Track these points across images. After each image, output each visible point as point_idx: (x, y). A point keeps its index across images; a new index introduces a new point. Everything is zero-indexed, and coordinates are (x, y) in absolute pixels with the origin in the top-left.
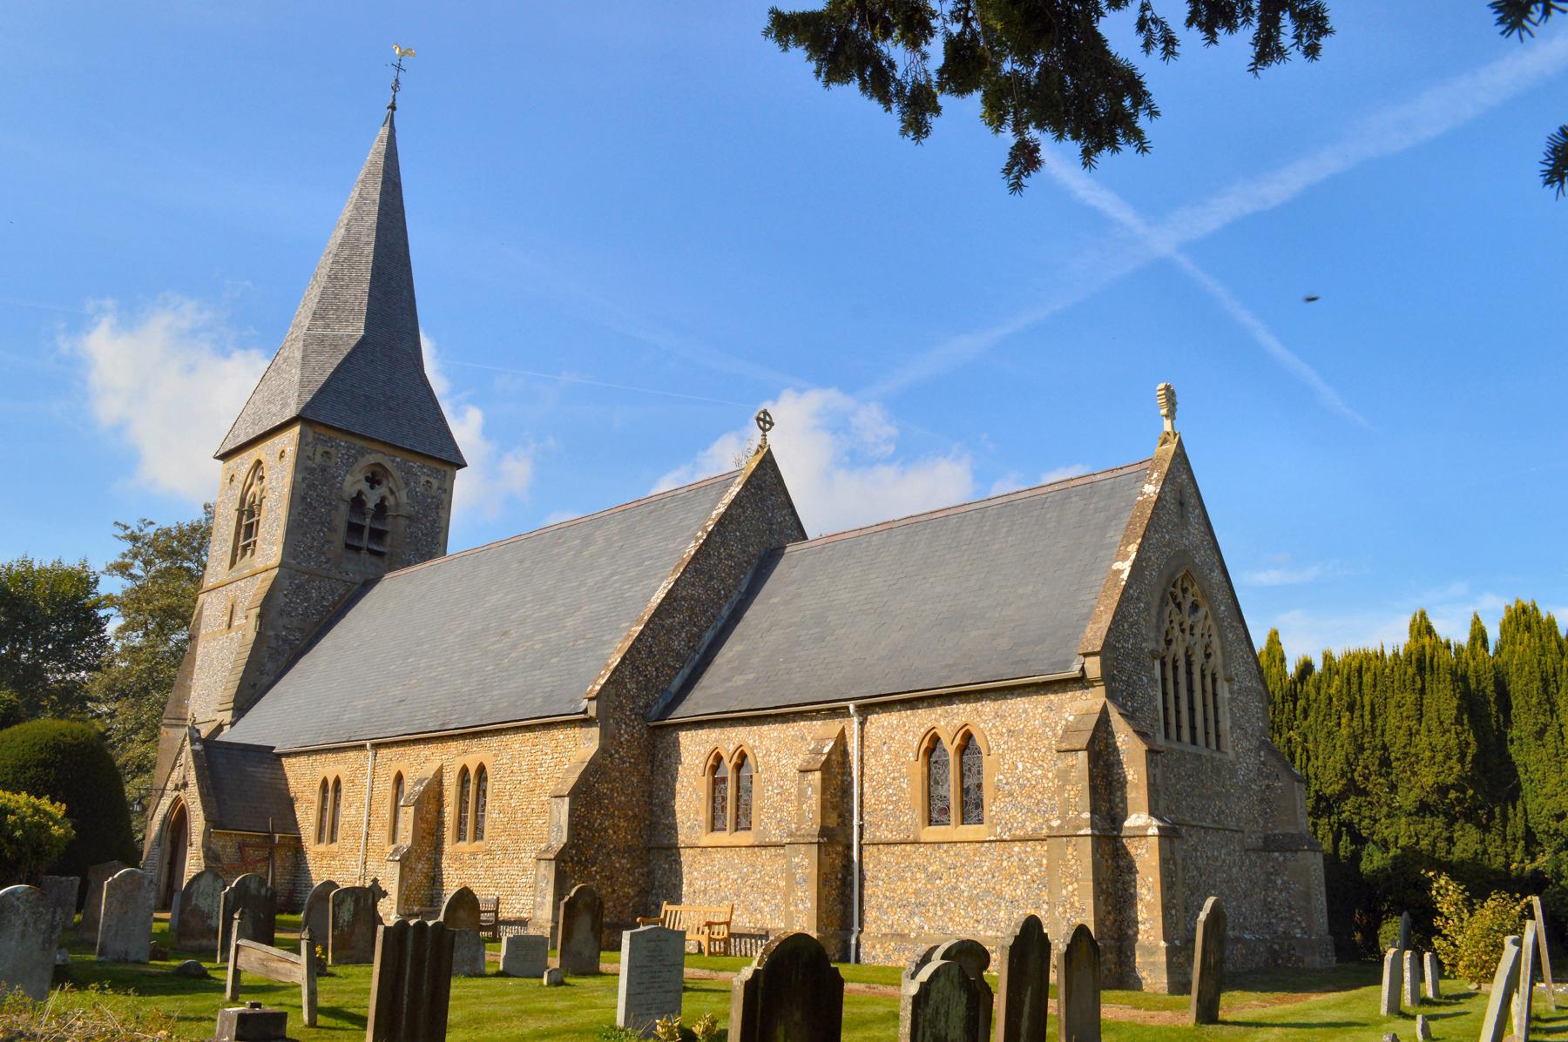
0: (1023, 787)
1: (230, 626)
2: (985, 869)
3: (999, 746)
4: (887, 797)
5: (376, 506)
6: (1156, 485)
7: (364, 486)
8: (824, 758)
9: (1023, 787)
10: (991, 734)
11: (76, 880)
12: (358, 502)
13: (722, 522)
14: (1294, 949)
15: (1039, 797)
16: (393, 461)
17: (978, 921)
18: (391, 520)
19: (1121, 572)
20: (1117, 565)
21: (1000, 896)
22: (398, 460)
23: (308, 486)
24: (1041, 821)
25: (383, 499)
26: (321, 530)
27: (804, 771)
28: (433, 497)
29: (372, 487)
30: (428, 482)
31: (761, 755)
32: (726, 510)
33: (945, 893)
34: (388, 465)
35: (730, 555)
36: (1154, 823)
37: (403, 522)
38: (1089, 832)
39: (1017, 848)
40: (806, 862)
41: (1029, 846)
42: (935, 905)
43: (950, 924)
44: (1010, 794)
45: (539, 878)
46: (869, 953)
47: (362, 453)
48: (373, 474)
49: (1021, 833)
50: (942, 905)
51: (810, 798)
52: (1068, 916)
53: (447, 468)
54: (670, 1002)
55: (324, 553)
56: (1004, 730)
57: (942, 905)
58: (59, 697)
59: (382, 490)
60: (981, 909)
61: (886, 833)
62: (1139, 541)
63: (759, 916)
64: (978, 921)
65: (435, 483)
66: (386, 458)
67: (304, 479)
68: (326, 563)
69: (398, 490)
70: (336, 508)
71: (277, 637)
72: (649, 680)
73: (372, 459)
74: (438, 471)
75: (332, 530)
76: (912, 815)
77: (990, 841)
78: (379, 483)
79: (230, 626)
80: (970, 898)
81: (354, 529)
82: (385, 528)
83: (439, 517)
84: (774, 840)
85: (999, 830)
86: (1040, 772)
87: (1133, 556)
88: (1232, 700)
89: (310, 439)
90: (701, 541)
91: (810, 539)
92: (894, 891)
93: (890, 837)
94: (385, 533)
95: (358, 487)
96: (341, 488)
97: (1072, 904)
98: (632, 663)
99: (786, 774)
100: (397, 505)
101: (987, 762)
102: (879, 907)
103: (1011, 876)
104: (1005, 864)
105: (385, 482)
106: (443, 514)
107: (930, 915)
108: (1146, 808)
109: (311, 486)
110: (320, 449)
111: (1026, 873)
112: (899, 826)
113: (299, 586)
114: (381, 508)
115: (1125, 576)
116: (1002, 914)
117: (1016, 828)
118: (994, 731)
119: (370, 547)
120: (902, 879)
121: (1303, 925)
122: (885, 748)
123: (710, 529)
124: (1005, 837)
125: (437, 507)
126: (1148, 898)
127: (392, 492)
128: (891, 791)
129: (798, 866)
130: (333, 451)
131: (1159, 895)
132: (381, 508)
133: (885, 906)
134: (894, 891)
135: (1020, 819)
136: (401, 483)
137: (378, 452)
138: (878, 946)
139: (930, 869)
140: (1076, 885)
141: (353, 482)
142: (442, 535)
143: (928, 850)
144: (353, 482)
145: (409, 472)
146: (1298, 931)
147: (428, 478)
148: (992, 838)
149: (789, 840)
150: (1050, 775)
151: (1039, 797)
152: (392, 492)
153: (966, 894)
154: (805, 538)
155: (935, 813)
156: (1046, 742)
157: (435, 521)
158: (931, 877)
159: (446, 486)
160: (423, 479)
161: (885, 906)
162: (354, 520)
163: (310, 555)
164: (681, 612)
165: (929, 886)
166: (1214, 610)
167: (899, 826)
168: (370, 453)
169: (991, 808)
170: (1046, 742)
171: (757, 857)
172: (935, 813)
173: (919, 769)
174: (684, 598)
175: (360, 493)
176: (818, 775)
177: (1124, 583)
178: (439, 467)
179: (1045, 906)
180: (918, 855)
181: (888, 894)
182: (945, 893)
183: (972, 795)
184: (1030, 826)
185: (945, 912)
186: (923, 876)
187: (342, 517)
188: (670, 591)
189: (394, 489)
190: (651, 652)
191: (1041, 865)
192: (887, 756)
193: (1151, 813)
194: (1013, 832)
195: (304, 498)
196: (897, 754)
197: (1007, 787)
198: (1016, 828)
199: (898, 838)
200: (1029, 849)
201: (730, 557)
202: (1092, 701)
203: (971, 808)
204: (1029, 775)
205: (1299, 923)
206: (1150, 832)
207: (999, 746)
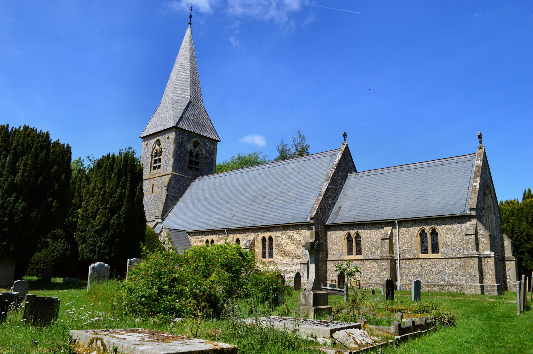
0: (451, 244)
1: (152, 192)
2: (440, 265)
3: (444, 233)
4: (408, 246)
5: (196, 154)
6: (481, 161)
7: (193, 148)
8: (389, 235)
9: (451, 244)
10: (441, 230)
11: (482, 259)
12: (191, 153)
13: (339, 165)
14: (511, 287)
15: (457, 246)
16: (201, 140)
17: (438, 279)
18: (200, 158)
19: (476, 186)
20: (474, 184)
21: (445, 273)
22: (202, 139)
23: (178, 148)
24: (457, 253)
25: (198, 152)
26: (182, 162)
27: (383, 239)
28: (212, 151)
29: (195, 148)
30: (210, 146)
31: (364, 234)
32: (339, 162)
33: (427, 272)
34: (199, 141)
35: (340, 175)
36: (493, 253)
37: (204, 159)
38: (493, 256)
39: (450, 260)
40: (386, 264)
41: (454, 260)
42: (425, 275)
43: (429, 280)
44: (448, 245)
45: (301, 269)
46: (403, 289)
47: (192, 138)
48: (195, 144)
49: (451, 256)
50: (427, 275)
51: (385, 246)
52: (471, 277)
53: (215, 142)
54: (58, 336)
55: (183, 169)
56: (445, 228)
57: (427, 275)
58: (526, 237)
59: (198, 149)
60: (439, 276)
61: (408, 256)
62: (480, 177)
63: (366, 279)
64: (438, 279)
65: (212, 146)
66: (199, 139)
67: (177, 146)
68: (184, 172)
69: (202, 149)
70: (186, 155)
71: (172, 196)
72: (324, 212)
73: (195, 139)
74: (213, 143)
75: (185, 162)
76: (416, 250)
77: (442, 258)
78: (196, 147)
79: (152, 192)
80: (436, 273)
81: (191, 162)
82: (199, 161)
83: (213, 157)
84: (370, 258)
85: (444, 255)
86: (457, 240)
87: (479, 182)
88: (495, 220)
89: (178, 133)
90: (333, 172)
91: (358, 172)
92: (411, 271)
93: (409, 257)
94: (199, 162)
95: (191, 148)
96: (187, 149)
97: (472, 274)
98: (320, 208)
99: (373, 239)
100: (202, 153)
101: (440, 238)
102: (406, 276)
103: (448, 267)
104: (446, 264)
105: (198, 146)
106: (214, 156)
107: (423, 278)
108: (490, 250)
109: (179, 148)
110: (181, 136)
111: (453, 266)
112: (412, 254)
113: (177, 180)
114: (197, 154)
115: (478, 187)
116: (446, 277)
117: (450, 255)
118: (442, 229)
119: (195, 167)
120: (414, 268)
121: (514, 280)
122: (407, 233)
123: (335, 168)
124: (446, 257)
125: (213, 154)
126: (491, 273)
127: (200, 150)
128: (409, 245)
129: (383, 265)
130: (184, 137)
131: (494, 272)
132: (197, 154)
133: (408, 275)
134: (411, 271)
135: (451, 252)
136: (203, 146)
137: (196, 137)
138: (407, 286)
139: (423, 265)
140: (473, 270)
141: (190, 147)
142: (214, 163)
143: (422, 260)
144: (190, 147)
145: (205, 143)
146: (512, 282)
147: (210, 145)
148: (442, 257)
149: (380, 258)
150: (460, 241)
151: (457, 246)
152: (200, 150)
153: (434, 272)
154: (356, 171)
155: (424, 250)
156: (459, 232)
157: (212, 159)
158: (423, 268)
159: (215, 147)
160: (209, 145)
161: (408, 275)
162: (190, 159)
163: (179, 170)
164: (330, 192)
165: (422, 270)
166: (491, 195)
167: (412, 254)
168: (194, 137)
169: (441, 249)
170: (459, 232)
171: (364, 262)
172: (424, 250)
173: (419, 238)
174: (330, 189)
175: (192, 150)
176: (388, 240)
177: (478, 189)
178: (213, 142)
179: (459, 275)
180: (419, 262)
181: (409, 272)
182: (427, 272)
183: (435, 246)
184: (454, 254)
185: (428, 277)
186: (420, 267)
187: (187, 158)
188: (328, 186)
189: (201, 148)
190: (324, 204)
191: (458, 264)
192: (407, 235)
193: (491, 251)
194: (449, 256)
195: (177, 152)
196: (411, 234)
197: (446, 244)
198: (450, 255)
199: (413, 257)
200: (454, 260)
201: (340, 176)
202: (474, 221)
203: (435, 249)
204: (453, 241)
205: (512, 280)
206: (491, 256)
207: (444, 233)
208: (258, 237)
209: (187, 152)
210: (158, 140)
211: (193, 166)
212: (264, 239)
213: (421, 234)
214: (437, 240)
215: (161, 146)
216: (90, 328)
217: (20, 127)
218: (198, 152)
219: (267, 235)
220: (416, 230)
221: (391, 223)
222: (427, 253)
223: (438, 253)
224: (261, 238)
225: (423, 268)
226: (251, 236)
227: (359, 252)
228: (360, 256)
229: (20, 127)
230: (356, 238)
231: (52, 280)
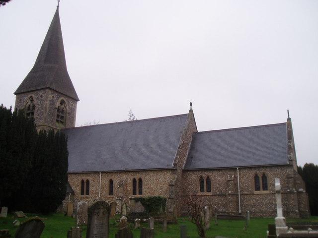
7: (60, 105)
12: (58, 109)
59: (63, 106)
73: (62, 98)
76: (252, 188)
81: (58, 116)
144: (58, 104)
172: (257, 189)
175: (59, 107)
187: (56, 113)
208: (129, 178)
209: (56, 108)
210: (31, 97)
211: (60, 119)
212: (134, 181)
213: (255, 177)
214: (266, 181)
215: (34, 103)
216: (6, 232)
217: (11, 107)
218: (63, 108)
219: (137, 177)
220: (252, 173)
221: (233, 169)
222: (260, 190)
223: (267, 190)
224: (132, 179)
225: (257, 201)
226: (124, 177)
227: (209, 190)
228: (210, 193)
229: (11, 107)
230: (207, 179)
231: (38, 131)
